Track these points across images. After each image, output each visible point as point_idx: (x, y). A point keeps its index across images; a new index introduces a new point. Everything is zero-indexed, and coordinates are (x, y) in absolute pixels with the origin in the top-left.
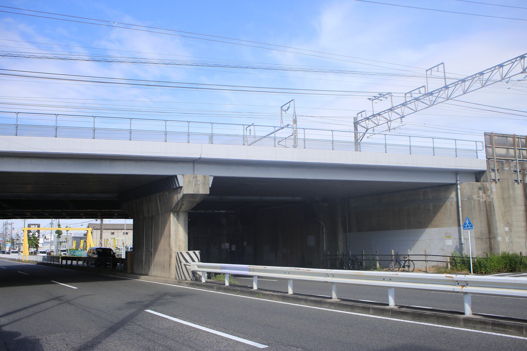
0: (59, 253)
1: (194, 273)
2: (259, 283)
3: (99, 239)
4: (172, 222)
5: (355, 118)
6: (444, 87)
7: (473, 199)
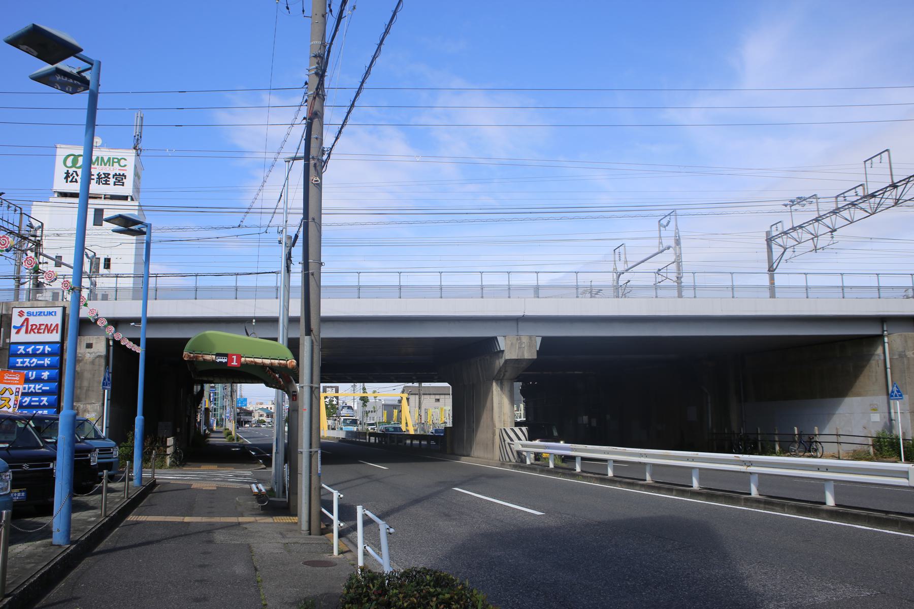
0: (366, 427)
1: (519, 453)
2: (615, 469)
3: (417, 409)
4: (495, 393)
5: (768, 233)
6: (890, 186)
7: (906, 356)
